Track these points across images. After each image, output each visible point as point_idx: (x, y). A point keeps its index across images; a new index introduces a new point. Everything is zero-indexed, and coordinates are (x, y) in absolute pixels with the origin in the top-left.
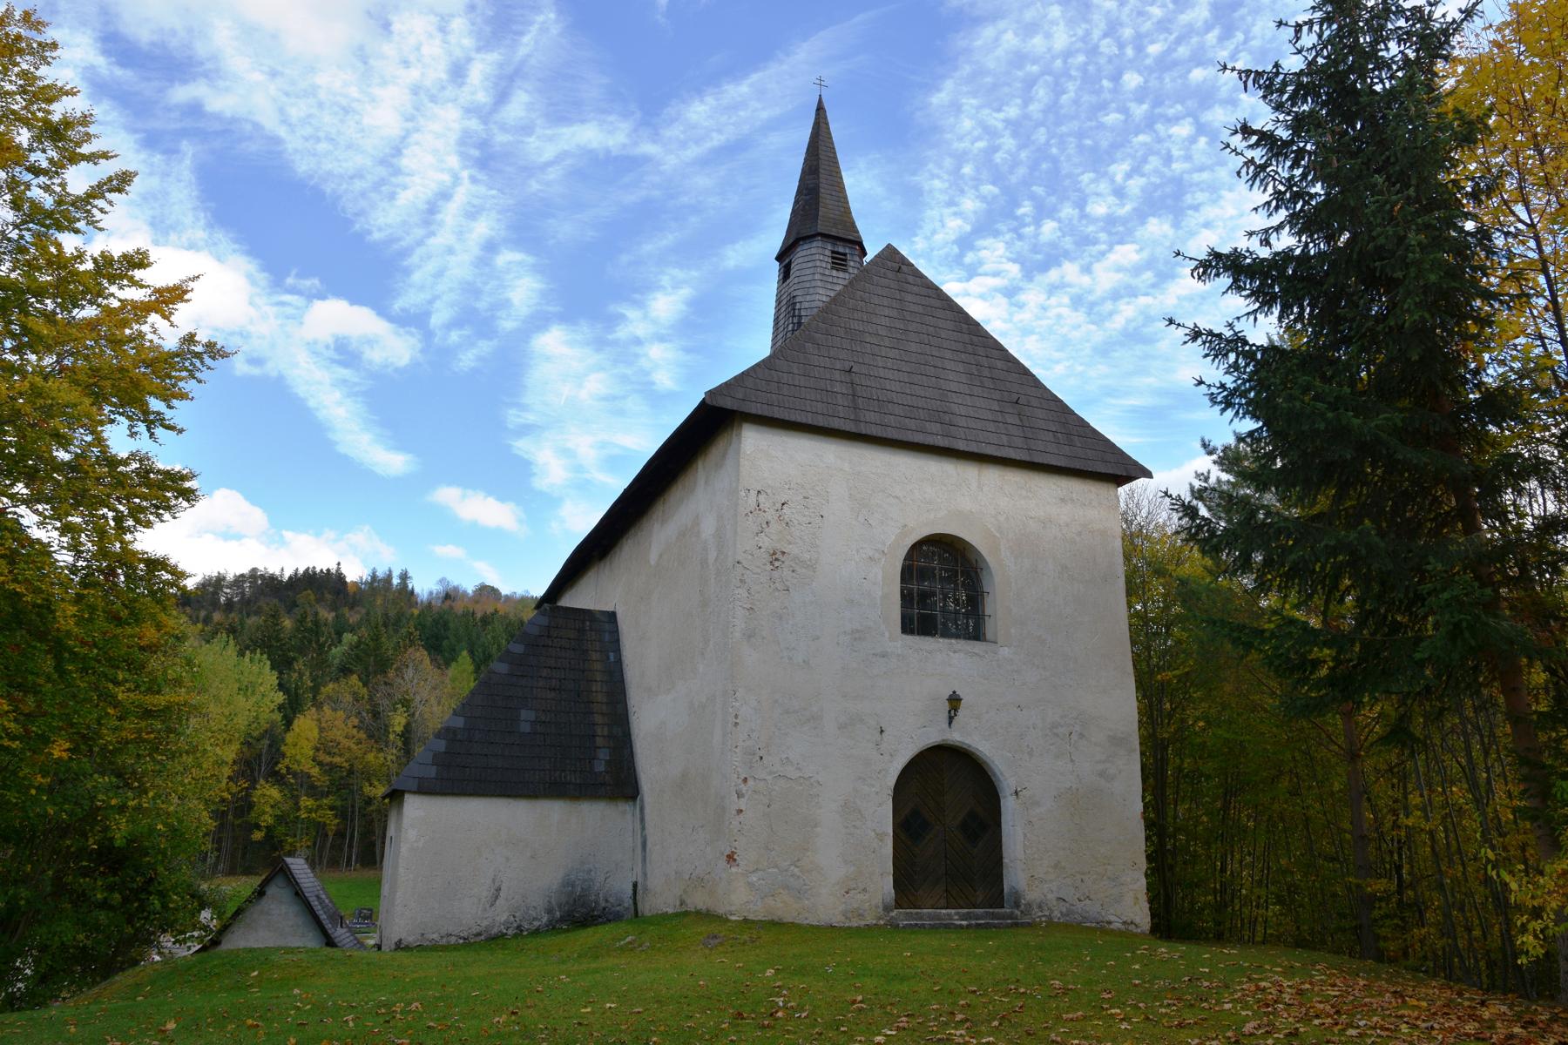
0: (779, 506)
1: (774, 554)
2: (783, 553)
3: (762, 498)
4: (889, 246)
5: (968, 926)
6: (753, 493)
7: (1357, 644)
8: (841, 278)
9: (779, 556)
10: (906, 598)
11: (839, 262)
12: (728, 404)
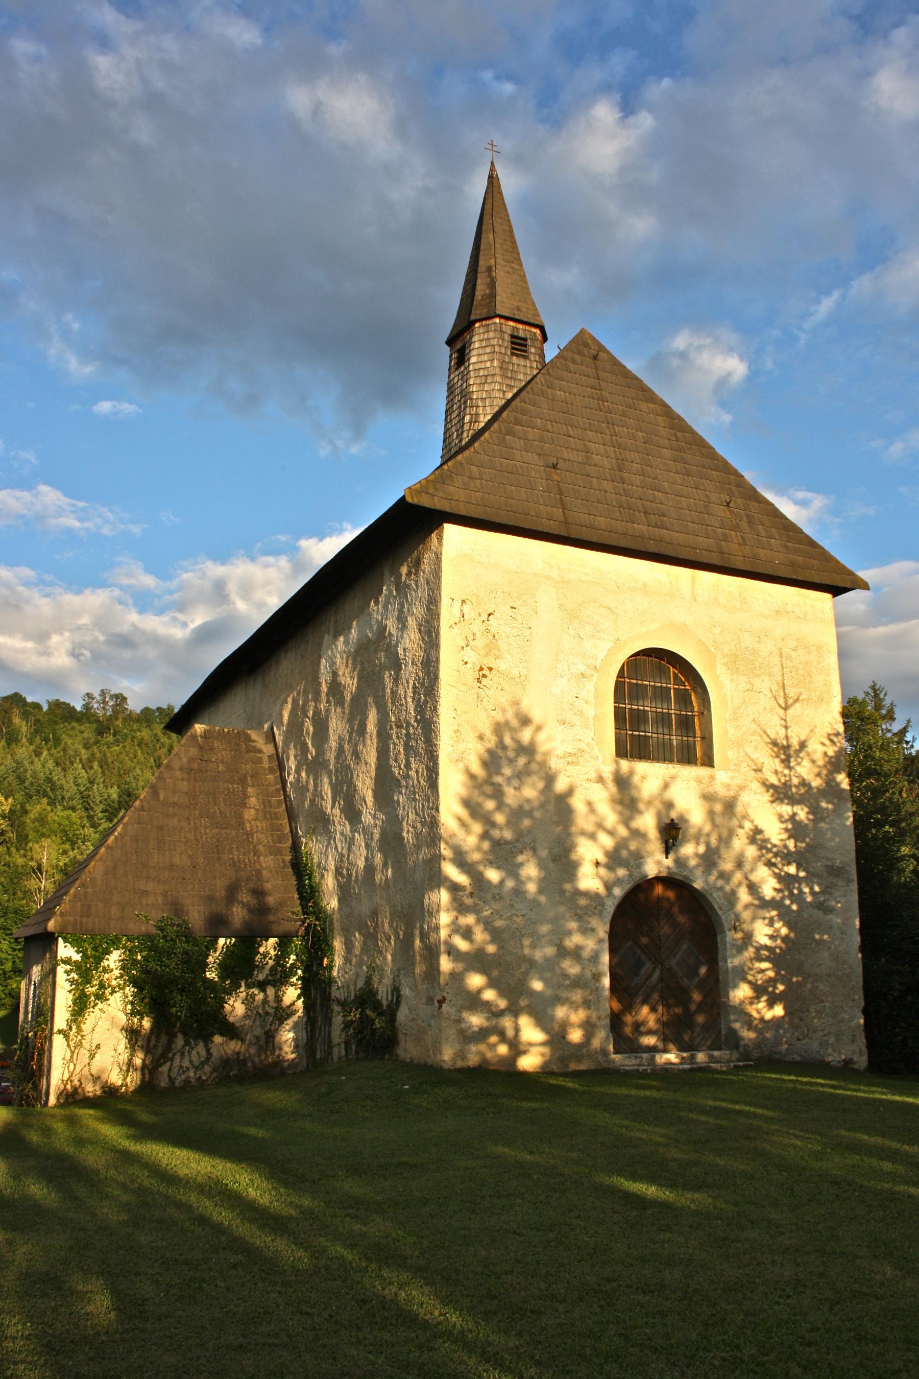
0: (485, 617)
1: (481, 669)
2: (490, 669)
3: (466, 608)
4: (582, 332)
5: (744, 1066)
6: (457, 604)
7: (249, 732)
8: (525, 369)
9: (486, 672)
10: (619, 715)
11: (519, 345)
12: (425, 501)
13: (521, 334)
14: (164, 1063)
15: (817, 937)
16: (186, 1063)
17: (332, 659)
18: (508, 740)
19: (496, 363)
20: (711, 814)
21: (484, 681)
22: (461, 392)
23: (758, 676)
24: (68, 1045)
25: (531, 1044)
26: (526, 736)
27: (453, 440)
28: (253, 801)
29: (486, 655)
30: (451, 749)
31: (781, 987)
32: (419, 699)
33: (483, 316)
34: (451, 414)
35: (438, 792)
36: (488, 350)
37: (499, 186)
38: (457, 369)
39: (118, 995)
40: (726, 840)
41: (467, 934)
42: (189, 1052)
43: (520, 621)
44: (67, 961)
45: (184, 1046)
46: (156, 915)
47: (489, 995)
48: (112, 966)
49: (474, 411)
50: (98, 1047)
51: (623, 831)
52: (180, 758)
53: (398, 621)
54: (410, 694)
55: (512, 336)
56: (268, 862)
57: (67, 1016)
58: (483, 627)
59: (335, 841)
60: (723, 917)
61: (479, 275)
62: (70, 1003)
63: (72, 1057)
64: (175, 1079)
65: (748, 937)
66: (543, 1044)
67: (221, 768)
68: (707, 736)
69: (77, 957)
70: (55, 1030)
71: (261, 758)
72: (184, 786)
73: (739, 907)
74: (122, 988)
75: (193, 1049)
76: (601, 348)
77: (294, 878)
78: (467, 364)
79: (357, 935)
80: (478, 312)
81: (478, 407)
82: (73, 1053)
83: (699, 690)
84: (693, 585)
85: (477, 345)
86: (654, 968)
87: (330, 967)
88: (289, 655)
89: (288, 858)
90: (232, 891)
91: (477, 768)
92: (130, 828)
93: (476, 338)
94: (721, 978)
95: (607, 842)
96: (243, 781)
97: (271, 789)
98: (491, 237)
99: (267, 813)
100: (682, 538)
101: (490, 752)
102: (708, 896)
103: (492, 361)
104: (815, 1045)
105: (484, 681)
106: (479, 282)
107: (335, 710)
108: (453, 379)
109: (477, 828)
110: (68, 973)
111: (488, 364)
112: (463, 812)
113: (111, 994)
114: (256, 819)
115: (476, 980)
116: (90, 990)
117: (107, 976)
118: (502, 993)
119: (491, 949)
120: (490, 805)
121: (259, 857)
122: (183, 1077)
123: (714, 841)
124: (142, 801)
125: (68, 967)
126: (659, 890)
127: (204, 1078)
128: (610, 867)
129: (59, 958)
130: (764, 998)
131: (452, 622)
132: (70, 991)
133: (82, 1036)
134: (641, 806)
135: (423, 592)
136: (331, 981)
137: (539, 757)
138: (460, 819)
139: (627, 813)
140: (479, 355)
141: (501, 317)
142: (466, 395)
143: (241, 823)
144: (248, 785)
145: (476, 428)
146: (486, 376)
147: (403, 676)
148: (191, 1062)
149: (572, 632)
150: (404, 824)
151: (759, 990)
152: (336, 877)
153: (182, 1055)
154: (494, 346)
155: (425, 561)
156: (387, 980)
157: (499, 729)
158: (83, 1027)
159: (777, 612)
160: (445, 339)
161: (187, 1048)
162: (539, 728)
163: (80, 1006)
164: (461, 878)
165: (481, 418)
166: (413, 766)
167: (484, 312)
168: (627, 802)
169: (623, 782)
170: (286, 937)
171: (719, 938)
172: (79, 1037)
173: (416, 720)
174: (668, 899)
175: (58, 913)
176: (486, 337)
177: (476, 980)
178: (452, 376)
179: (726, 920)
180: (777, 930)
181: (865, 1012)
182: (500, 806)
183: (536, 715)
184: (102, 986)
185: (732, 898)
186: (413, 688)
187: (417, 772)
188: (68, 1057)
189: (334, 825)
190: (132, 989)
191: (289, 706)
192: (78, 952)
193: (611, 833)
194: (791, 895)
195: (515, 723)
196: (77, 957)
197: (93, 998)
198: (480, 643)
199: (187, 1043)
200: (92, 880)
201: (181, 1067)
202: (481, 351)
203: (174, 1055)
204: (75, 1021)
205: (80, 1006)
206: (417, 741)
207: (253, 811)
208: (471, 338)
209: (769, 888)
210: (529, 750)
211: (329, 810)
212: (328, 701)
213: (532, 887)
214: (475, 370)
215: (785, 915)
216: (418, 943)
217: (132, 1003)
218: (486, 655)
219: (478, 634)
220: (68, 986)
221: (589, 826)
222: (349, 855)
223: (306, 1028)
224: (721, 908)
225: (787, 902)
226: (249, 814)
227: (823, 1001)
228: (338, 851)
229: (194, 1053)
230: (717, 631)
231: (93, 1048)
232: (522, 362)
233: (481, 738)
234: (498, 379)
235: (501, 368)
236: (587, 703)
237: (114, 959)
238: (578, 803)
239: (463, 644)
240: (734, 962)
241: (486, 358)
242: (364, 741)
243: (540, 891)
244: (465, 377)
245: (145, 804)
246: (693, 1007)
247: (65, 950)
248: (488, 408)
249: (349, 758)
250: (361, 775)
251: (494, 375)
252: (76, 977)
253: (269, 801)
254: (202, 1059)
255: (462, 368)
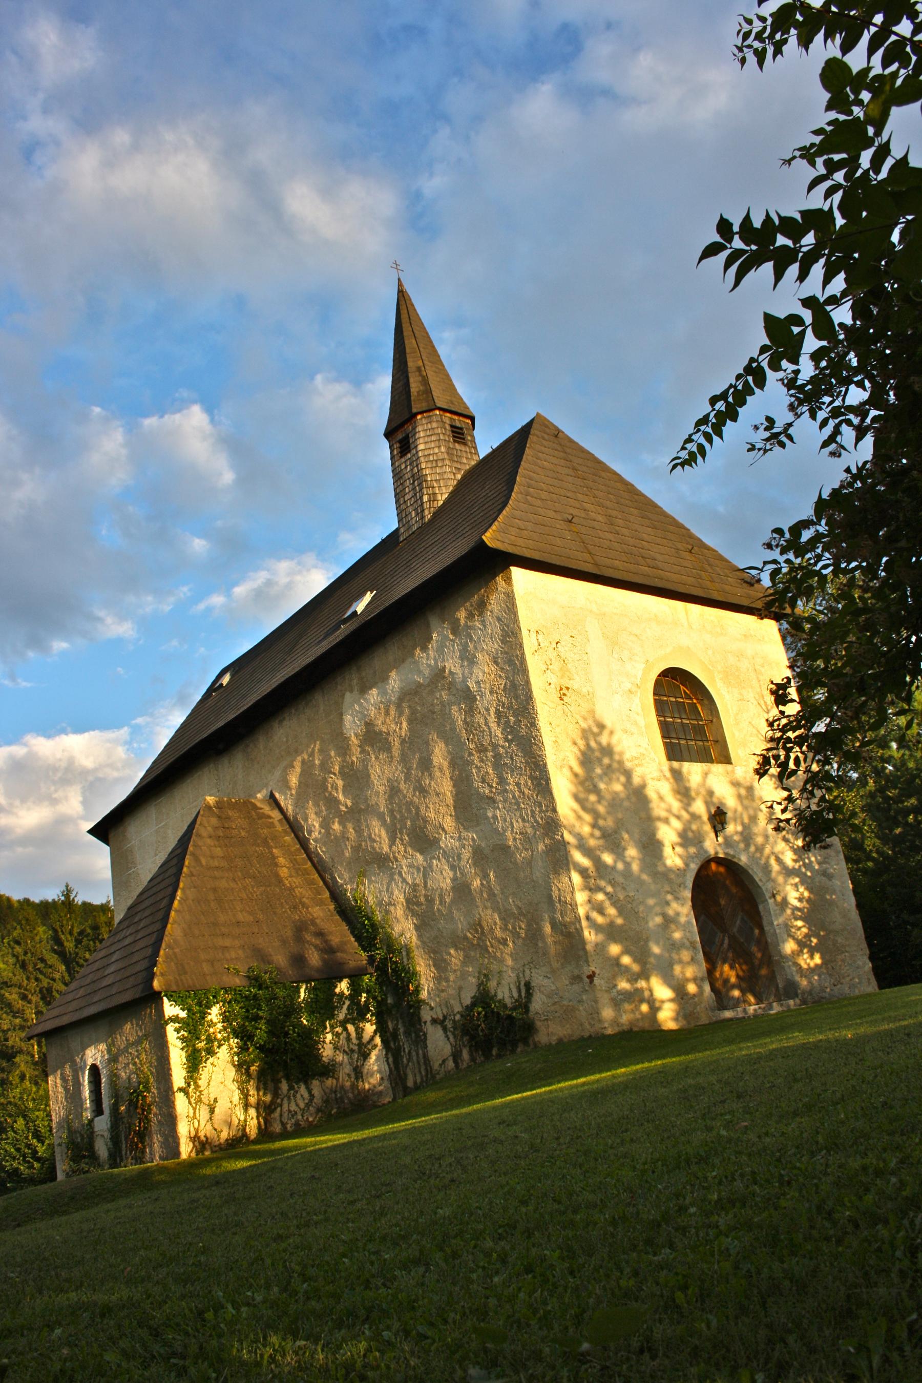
0: (554, 645)
1: (561, 689)
2: (568, 688)
3: (541, 637)
6: (533, 635)
9: (564, 691)
13: (458, 424)
14: (275, 1109)
15: (828, 897)
16: (293, 1107)
17: (362, 713)
18: (593, 744)
19: (443, 449)
20: (739, 797)
21: (565, 698)
22: (413, 476)
23: (744, 688)
24: (190, 1103)
25: (663, 1002)
26: (604, 740)
27: (412, 519)
28: (281, 860)
29: (562, 677)
30: (554, 757)
31: (814, 941)
32: (508, 722)
33: (424, 409)
34: (403, 497)
35: (551, 794)
36: (434, 438)
37: (410, 300)
38: (401, 457)
39: (224, 1047)
40: (754, 819)
41: (601, 910)
42: (294, 1096)
43: (579, 648)
44: (175, 1019)
45: (289, 1090)
46: (243, 969)
47: (626, 960)
48: (215, 1020)
49: (430, 491)
50: (216, 1100)
51: (685, 816)
52: (205, 827)
53: (462, 660)
54: (492, 719)
55: (452, 426)
56: (317, 912)
57: (184, 1073)
58: (555, 654)
59: (400, 874)
60: (764, 888)
61: (410, 375)
62: (184, 1060)
63: (194, 1113)
64: (287, 1123)
65: (785, 902)
66: (672, 1000)
67: (243, 834)
68: (719, 739)
69: (183, 1014)
70: (175, 1089)
71: (272, 823)
72: (219, 851)
73: (773, 874)
74: (227, 1039)
75: (297, 1092)
76: (559, 431)
77: (344, 923)
78: (414, 451)
79: (452, 951)
80: (418, 406)
81: (433, 487)
82: (194, 1109)
83: (706, 702)
84: (687, 614)
85: (422, 434)
86: (724, 936)
87: (417, 991)
88: (286, 723)
89: (332, 907)
90: (299, 938)
91: (578, 769)
92: (188, 892)
93: (420, 428)
94: (769, 940)
95: (677, 824)
96: (265, 842)
97: (293, 849)
98: (414, 341)
99: (296, 868)
100: (675, 577)
101: (583, 754)
102: (750, 871)
103: (439, 447)
104: (846, 990)
105: (565, 698)
106: (411, 380)
107: (377, 758)
108: (399, 466)
109: (588, 818)
110: (177, 1031)
111: (436, 450)
112: (576, 806)
113: (219, 1047)
114: (291, 876)
115: (615, 949)
116: (201, 1045)
117: (211, 1030)
118: (636, 960)
119: (619, 921)
120: (593, 798)
121: (307, 908)
122: (293, 1121)
123: (746, 820)
124: (188, 867)
125: (177, 1025)
126: (713, 866)
127: (311, 1119)
128: (682, 845)
129: (167, 1017)
130: (805, 951)
131: (533, 650)
132: (182, 1049)
133: (200, 1092)
134: (693, 794)
135: (494, 628)
136: (419, 1004)
137: (617, 757)
138: (575, 811)
139: (685, 800)
140: (426, 443)
141: (440, 409)
142: (419, 479)
143: (280, 881)
144: (272, 847)
145: (435, 505)
146: (436, 461)
147: (480, 706)
148: (297, 1105)
149: (616, 656)
150: (508, 834)
151: (802, 944)
152: (408, 907)
153: (289, 1099)
154: (438, 434)
155: (492, 602)
156: (510, 977)
157: (586, 734)
158: (200, 1082)
159: (745, 636)
160: (543, 413)
161: (292, 1092)
162: (612, 733)
163: (194, 1064)
164: (585, 862)
165: (439, 497)
166: (511, 780)
167: (424, 406)
168: (683, 791)
169: (677, 775)
170: (356, 976)
171: (761, 907)
172: (198, 1093)
173: (506, 740)
174: (721, 873)
175: (158, 973)
176: (429, 426)
177: (615, 949)
178: (397, 464)
179: (766, 887)
180: (802, 894)
181: (871, 958)
182: (600, 798)
183: (608, 723)
184: (210, 1040)
185: (767, 869)
186: (496, 713)
187: (518, 784)
188: (191, 1114)
189: (397, 860)
190: (236, 1041)
191: (298, 769)
192: (183, 1010)
193: (678, 817)
194: (804, 865)
195: (595, 730)
196: (183, 1014)
197: (204, 1054)
198: (556, 666)
199: (291, 1088)
200: (175, 941)
201: (290, 1111)
202: (427, 439)
203: (282, 1100)
204: (191, 1077)
205: (194, 1064)
206: (512, 758)
207: (285, 870)
208: (414, 429)
209: (789, 858)
210: (608, 751)
211: (386, 849)
212: (363, 751)
213: (635, 867)
214: (425, 456)
215: (804, 880)
216: (548, 929)
217: (238, 1054)
218: (562, 677)
219: (554, 660)
220: (179, 1044)
221: (663, 814)
222: (425, 883)
223: (387, 1061)
224: (761, 880)
225: (803, 870)
226: (284, 872)
227: (843, 952)
228: (407, 883)
229: (298, 1096)
230: (710, 652)
231: (212, 1102)
232: (463, 448)
233: (575, 743)
234: (448, 463)
235: (448, 453)
236: (638, 714)
237: (214, 1013)
238: (651, 793)
239: (544, 668)
240: (778, 921)
241: (433, 445)
242: (430, 775)
243: (642, 870)
244: (416, 462)
245: (192, 869)
246: (757, 962)
247: (170, 1009)
248: (443, 488)
249: (409, 795)
250: (431, 806)
251: (443, 460)
252: (186, 1034)
253: (295, 860)
254: (306, 1101)
255: (409, 456)
